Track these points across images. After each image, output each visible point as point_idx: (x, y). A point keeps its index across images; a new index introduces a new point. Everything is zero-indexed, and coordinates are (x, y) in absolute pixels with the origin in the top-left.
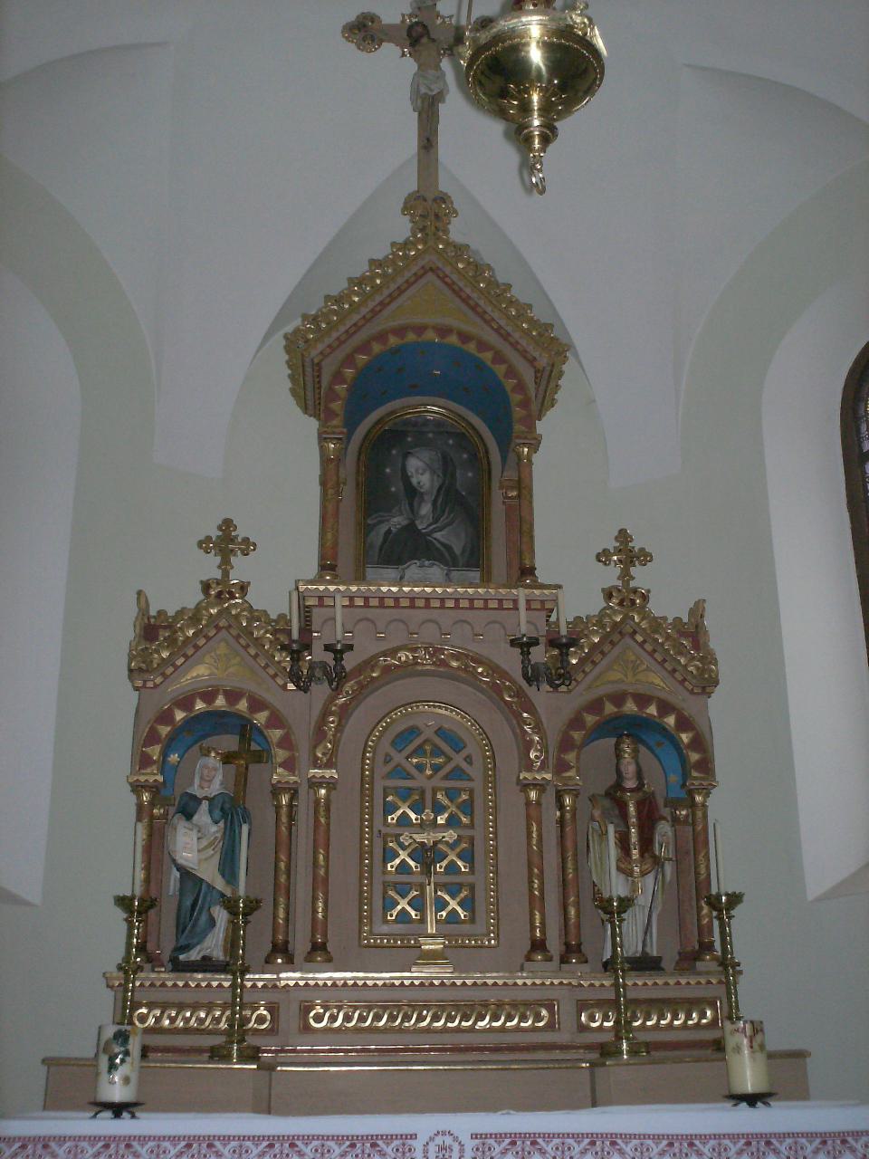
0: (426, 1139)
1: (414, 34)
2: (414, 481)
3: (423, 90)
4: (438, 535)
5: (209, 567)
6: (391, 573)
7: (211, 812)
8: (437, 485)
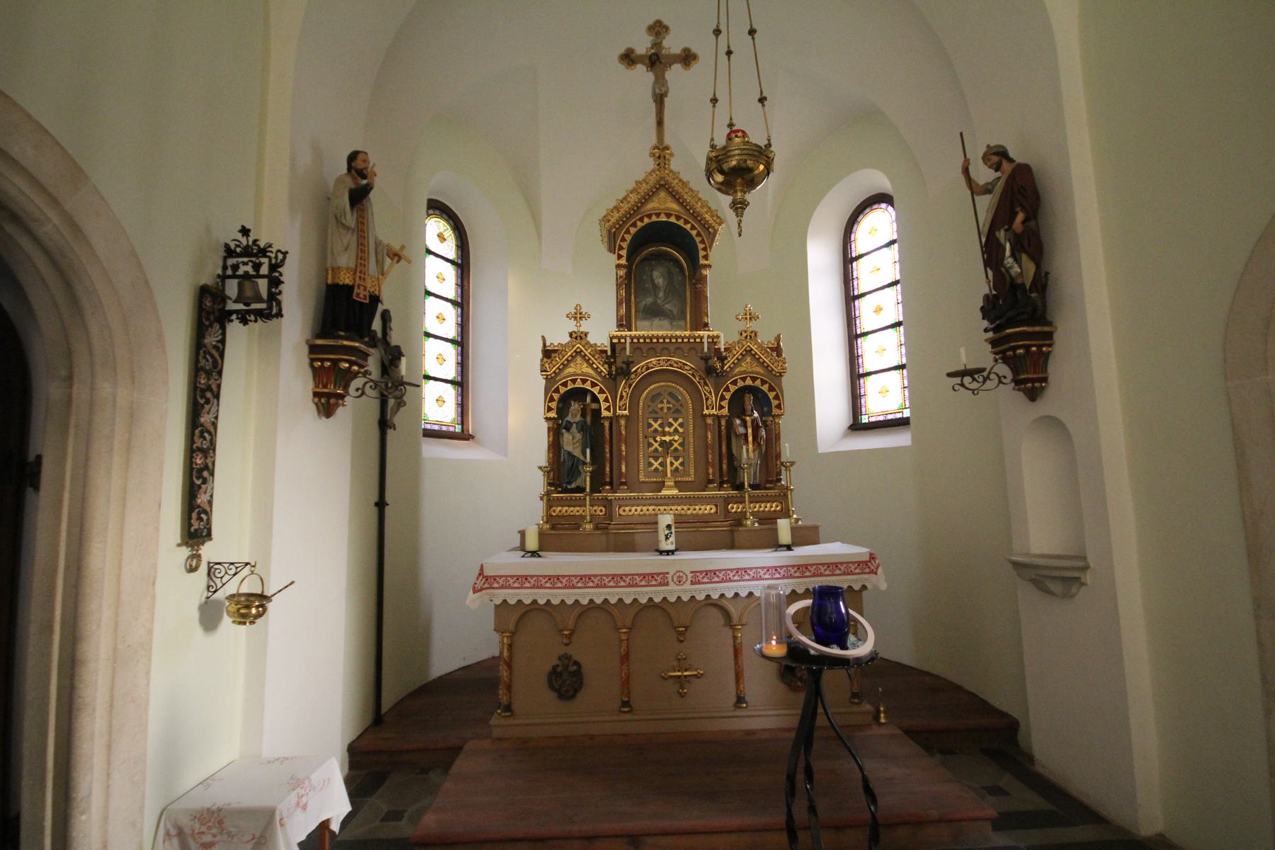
0: (672, 574)
1: (653, 60)
2: (656, 282)
3: (657, 91)
4: (667, 306)
5: (572, 326)
6: (646, 323)
7: (577, 428)
8: (666, 284)
